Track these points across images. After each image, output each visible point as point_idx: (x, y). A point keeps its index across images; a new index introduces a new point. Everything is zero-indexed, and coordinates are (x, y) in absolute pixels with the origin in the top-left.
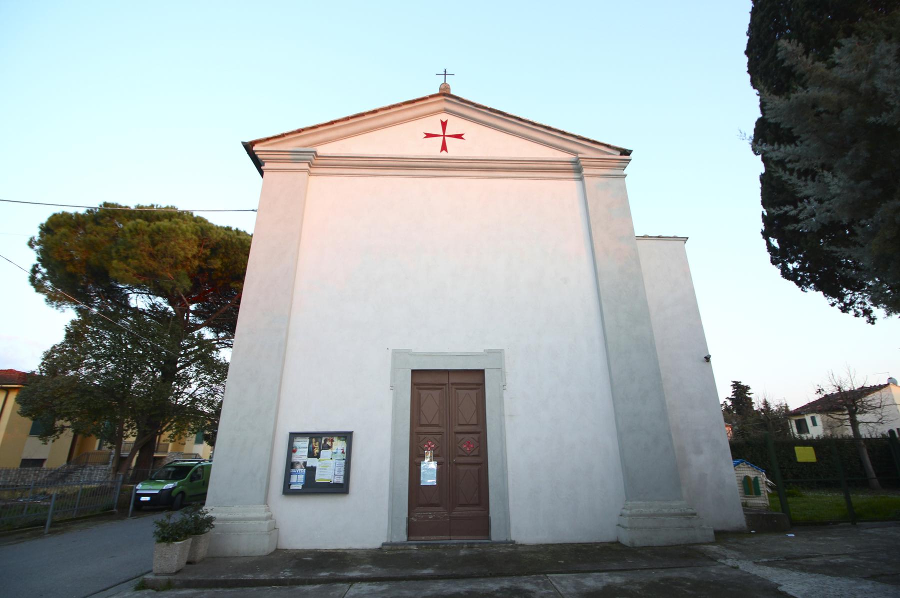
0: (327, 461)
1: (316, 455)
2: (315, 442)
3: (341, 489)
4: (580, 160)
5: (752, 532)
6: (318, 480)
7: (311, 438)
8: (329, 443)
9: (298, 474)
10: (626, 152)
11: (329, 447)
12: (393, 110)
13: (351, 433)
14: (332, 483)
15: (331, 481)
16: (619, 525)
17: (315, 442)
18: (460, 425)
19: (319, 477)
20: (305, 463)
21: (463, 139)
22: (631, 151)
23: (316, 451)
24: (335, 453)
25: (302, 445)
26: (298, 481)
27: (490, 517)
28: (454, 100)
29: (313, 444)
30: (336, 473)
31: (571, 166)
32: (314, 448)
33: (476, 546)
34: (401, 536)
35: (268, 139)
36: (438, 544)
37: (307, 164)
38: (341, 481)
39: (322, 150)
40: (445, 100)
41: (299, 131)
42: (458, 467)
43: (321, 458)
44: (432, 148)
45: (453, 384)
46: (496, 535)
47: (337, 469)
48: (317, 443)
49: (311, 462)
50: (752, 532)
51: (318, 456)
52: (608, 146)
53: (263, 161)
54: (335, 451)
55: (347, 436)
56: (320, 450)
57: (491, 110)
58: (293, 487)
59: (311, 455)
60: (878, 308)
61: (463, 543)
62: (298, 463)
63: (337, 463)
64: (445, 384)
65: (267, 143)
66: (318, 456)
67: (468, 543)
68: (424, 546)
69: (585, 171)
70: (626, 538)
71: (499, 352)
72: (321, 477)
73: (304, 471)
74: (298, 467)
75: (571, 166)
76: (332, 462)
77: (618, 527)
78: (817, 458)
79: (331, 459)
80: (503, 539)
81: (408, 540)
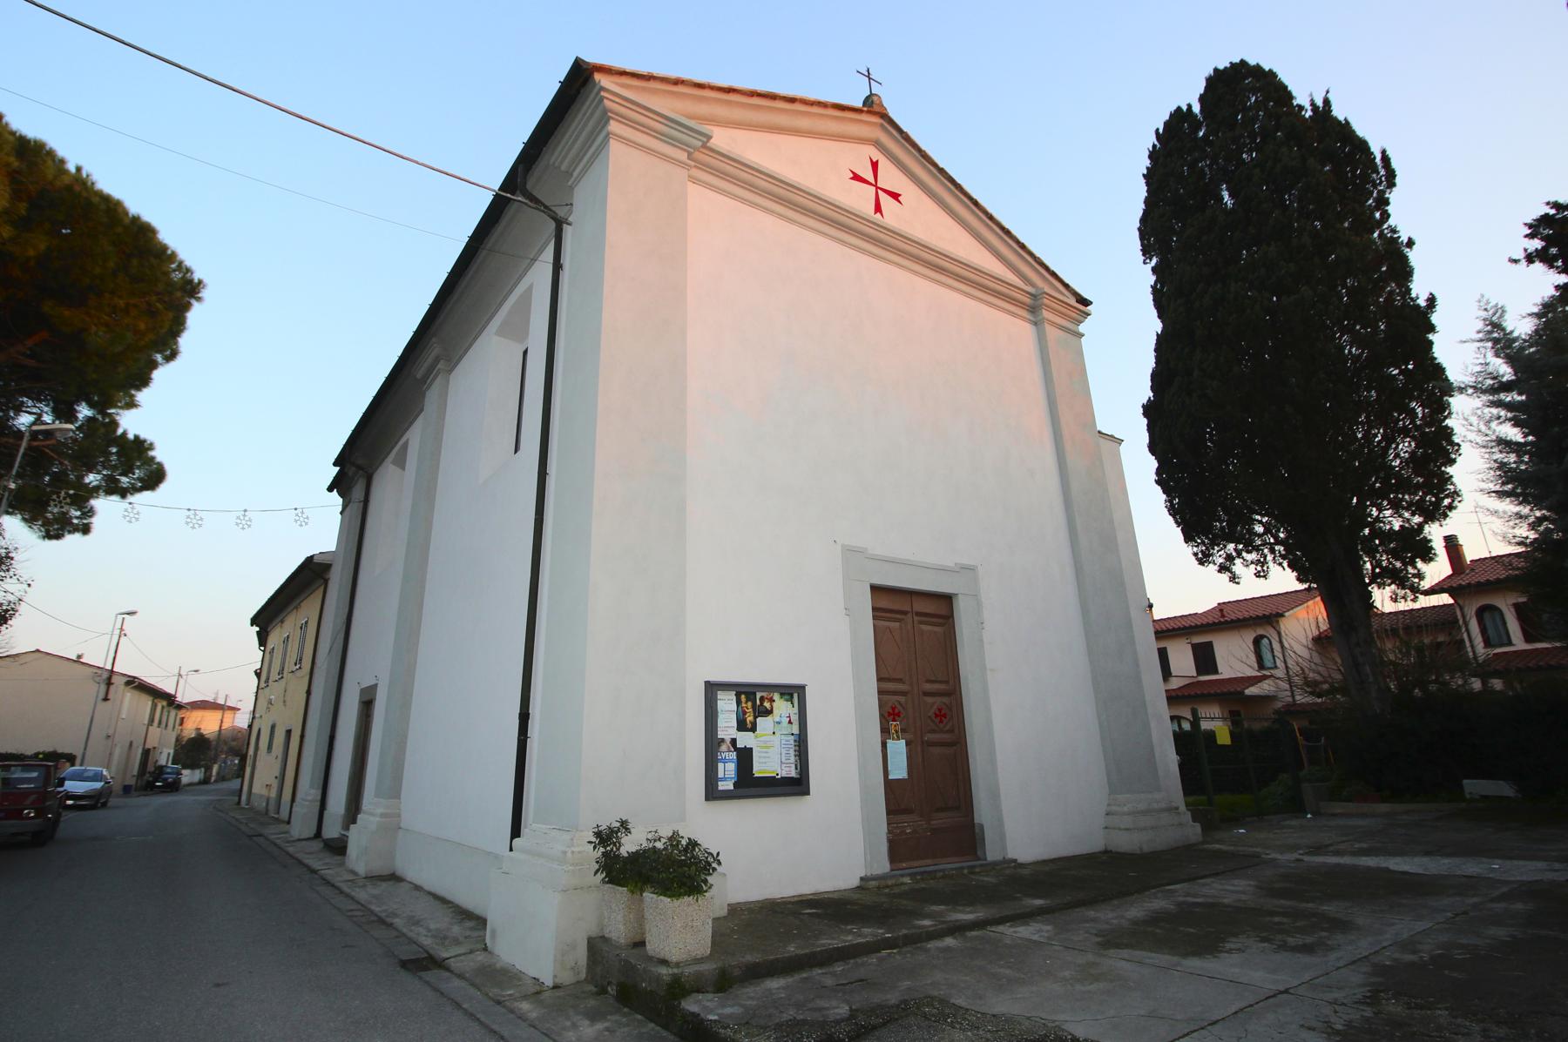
0: (768, 738)
1: (749, 726)
2: (746, 703)
3: (797, 785)
4: (1045, 296)
5: (158, 784)
6: (760, 771)
7: (738, 695)
8: (767, 704)
9: (725, 761)
10: (1085, 302)
11: (769, 712)
12: (815, 110)
13: (707, 683)
14: (779, 777)
15: (777, 775)
16: (1106, 828)
17: (746, 703)
18: (928, 681)
19: (761, 768)
20: (734, 741)
21: (899, 202)
22: (1091, 303)
23: (750, 718)
24: (779, 723)
25: (727, 704)
26: (728, 770)
27: (982, 827)
28: (895, 133)
29: (744, 705)
30: (783, 760)
31: (1028, 300)
32: (745, 713)
33: (977, 870)
34: (883, 866)
35: (623, 73)
36: (936, 871)
37: (686, 154)
38: (793, 773)
39: (722, 139)
40: (882, 125)
41: (678, 82)
42: (931, 748)
43: (758, 732)
44: (860, 199)
45: (918, 614)
46: (992, 854)
47: (784, 751)
48: (750, 704)
49: (745, 739)
50: (158, 784)
51: (753, 729)
52: (1066, 286)
53: (610, 114)
54: (777, 719)
55: (794, 692)
56: (755, 718)
57: (942, 171)
58: (723, 786)
59: (742, 726)
60: (86, 530)
61: (962, 868)
62: (723, 740)
63: (783, 742)
64: (905, 613)
65: (625, 80)
66: (753, 729)
67: (968, 867)
68: (919, 877)
69: (1045, 314)
70: (1126, 842)
71: (971, 569)
72: (764, 766)
73: (734, 755)
74: (724, 747)
75: (1028, 300)
76: (776, 738)
77: (1107, 830)
78: (1232, 741)
79: (774, 733)
80: (1000, 858)
81: (892, 870)
